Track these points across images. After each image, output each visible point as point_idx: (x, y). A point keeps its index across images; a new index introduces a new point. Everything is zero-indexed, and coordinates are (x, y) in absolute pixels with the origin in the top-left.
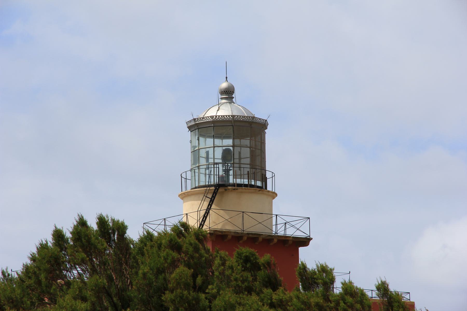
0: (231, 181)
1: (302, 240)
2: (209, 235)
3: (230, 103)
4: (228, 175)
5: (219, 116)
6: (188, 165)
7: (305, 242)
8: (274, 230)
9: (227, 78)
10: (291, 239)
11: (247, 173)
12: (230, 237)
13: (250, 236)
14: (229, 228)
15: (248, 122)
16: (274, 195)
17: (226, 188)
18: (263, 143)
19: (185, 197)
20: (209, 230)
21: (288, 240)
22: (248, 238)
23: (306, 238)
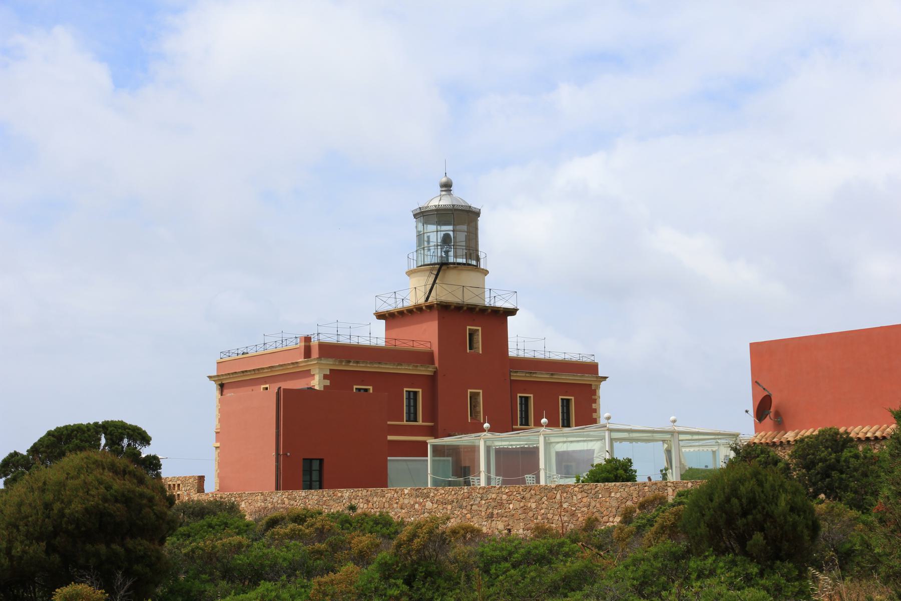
4: (447, 256)
16: (486, 272)
18: (476, 229)
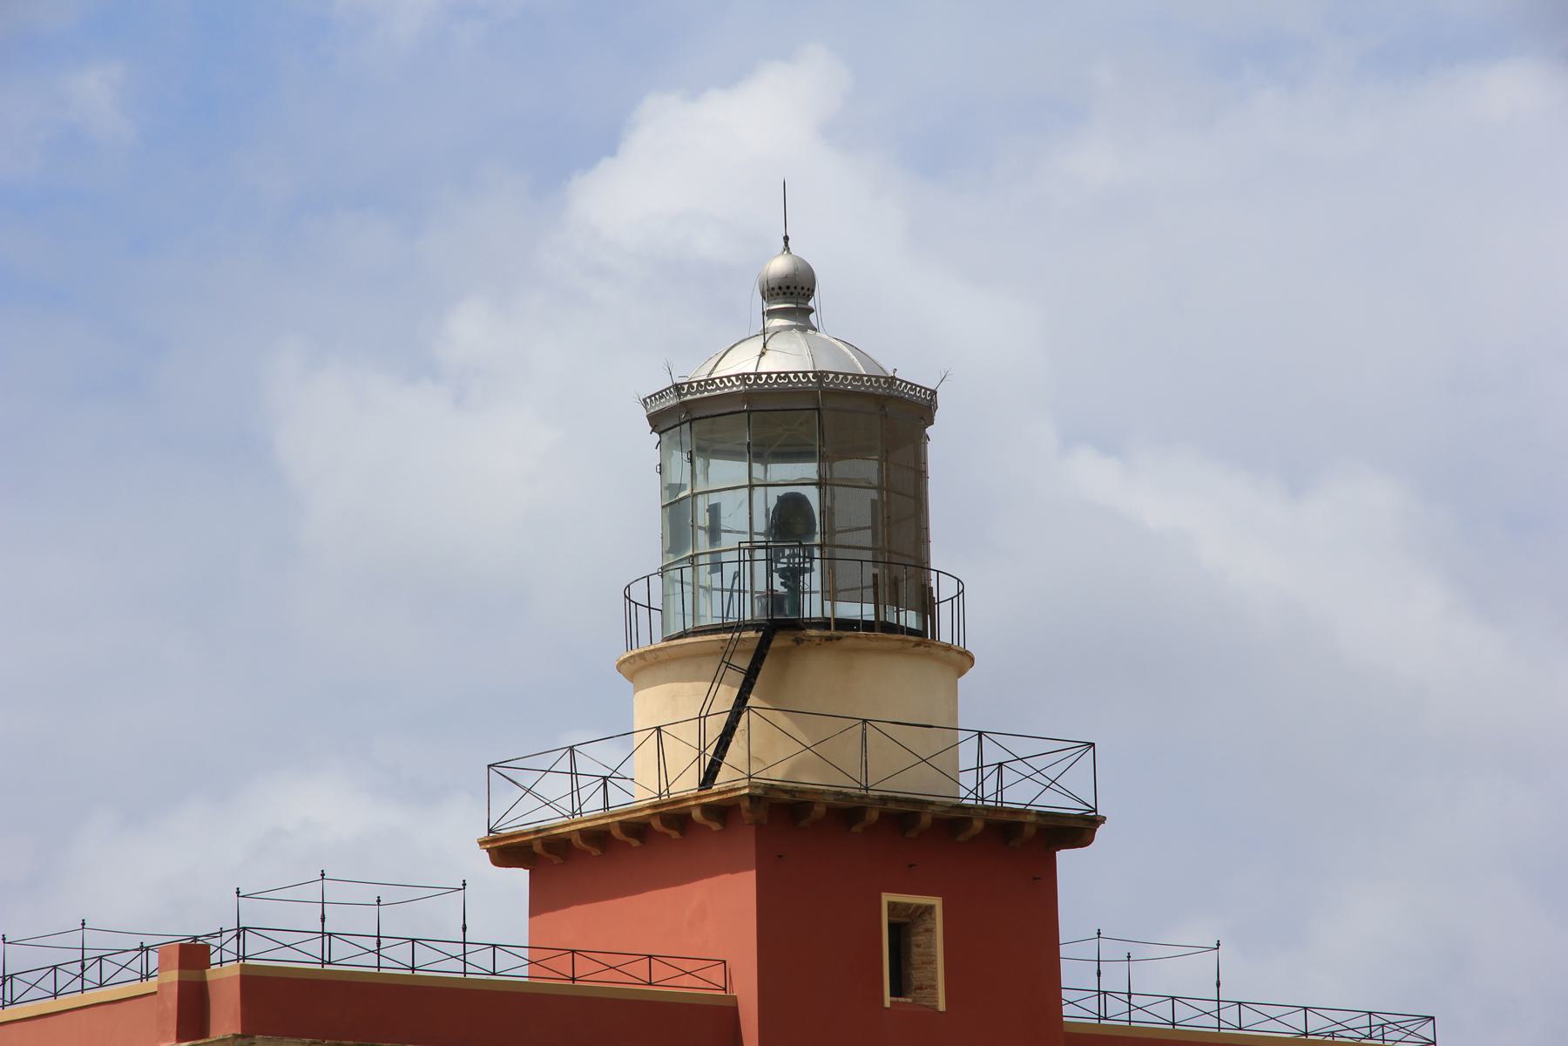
0: (813, 607)
1: (1072, 824)
2: (746, 804)
3: (803, 330)
5: (769, 374)
6: (651, 553)
7: (1079, 829)
8: (968, 780)
9: (786, 238)
10: (1031, 819)
11: (870, 583)
12: (820, 810)
13: (891, 806)
14: (812, 778)
15: (872, 395)
16: (961, 660)
17: (800, 634)
18: (920, 474)
19: (642, 668)
20: (749, 786)
21: (1021, 824)
22: (884, 815)
23: (1082, 817)
